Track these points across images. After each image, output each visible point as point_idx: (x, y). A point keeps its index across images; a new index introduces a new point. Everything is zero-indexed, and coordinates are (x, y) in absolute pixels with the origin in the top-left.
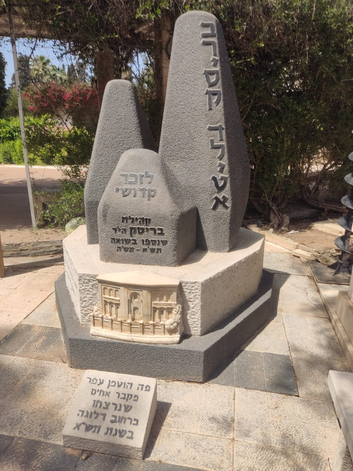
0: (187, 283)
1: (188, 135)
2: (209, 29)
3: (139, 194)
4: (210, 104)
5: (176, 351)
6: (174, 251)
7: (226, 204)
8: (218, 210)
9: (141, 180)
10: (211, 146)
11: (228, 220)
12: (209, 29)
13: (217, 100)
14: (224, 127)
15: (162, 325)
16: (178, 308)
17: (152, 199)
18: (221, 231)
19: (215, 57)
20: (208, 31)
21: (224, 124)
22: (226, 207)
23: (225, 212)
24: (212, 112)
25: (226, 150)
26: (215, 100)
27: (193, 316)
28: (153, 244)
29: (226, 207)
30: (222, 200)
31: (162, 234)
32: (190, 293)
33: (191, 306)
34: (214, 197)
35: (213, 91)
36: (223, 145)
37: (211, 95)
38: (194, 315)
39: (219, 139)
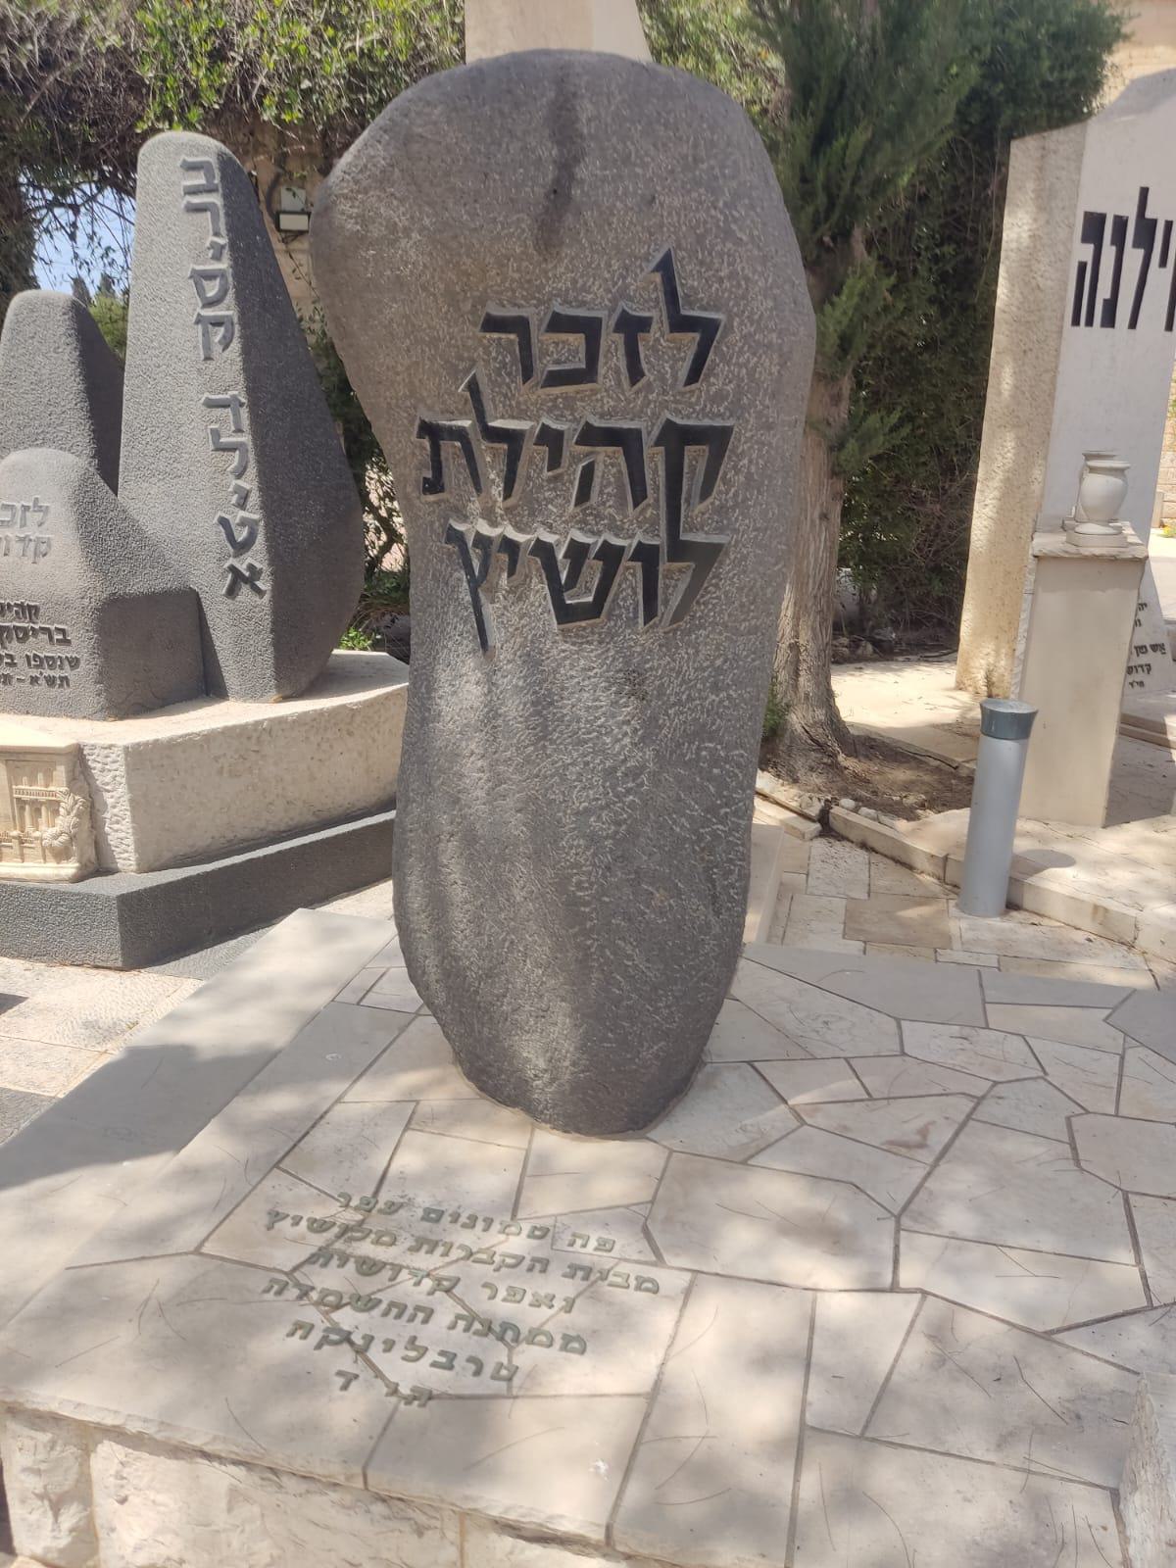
0: (94, 747)
1: (168, 419)
2: (202, 173)
3: (16, 548)
4: (207, 346)
5: (63, 896)
6: (95, 682)
7: (259, 584)
8: (239, 598)
9: (24, 518)
10: (214, 443)
11: (267, 623)
12: (202, 173)
13: (224, 337)
14: (243, 400)
15: (37, 838)
16: (70, 805)
17: (42, 560)
18: (252, 649)
19: (216, 239)
20: (200, 180)
21: (243, 394)
22: (260, 592)
23: (257, 604)
24: (212, 365)
25: (251, 456)
26: (217, 339)
27: (116, 827)
28: (51, 667)
29: (260, 592)
30: (247, 574)
31: (66, 642)
32: (103, 770)
33: (110, 801)
34: (226, 565)
35: (215, 317)
36: (242, 444)
37: (210, 326)
38: (117, 822)
39: (233, 428)
